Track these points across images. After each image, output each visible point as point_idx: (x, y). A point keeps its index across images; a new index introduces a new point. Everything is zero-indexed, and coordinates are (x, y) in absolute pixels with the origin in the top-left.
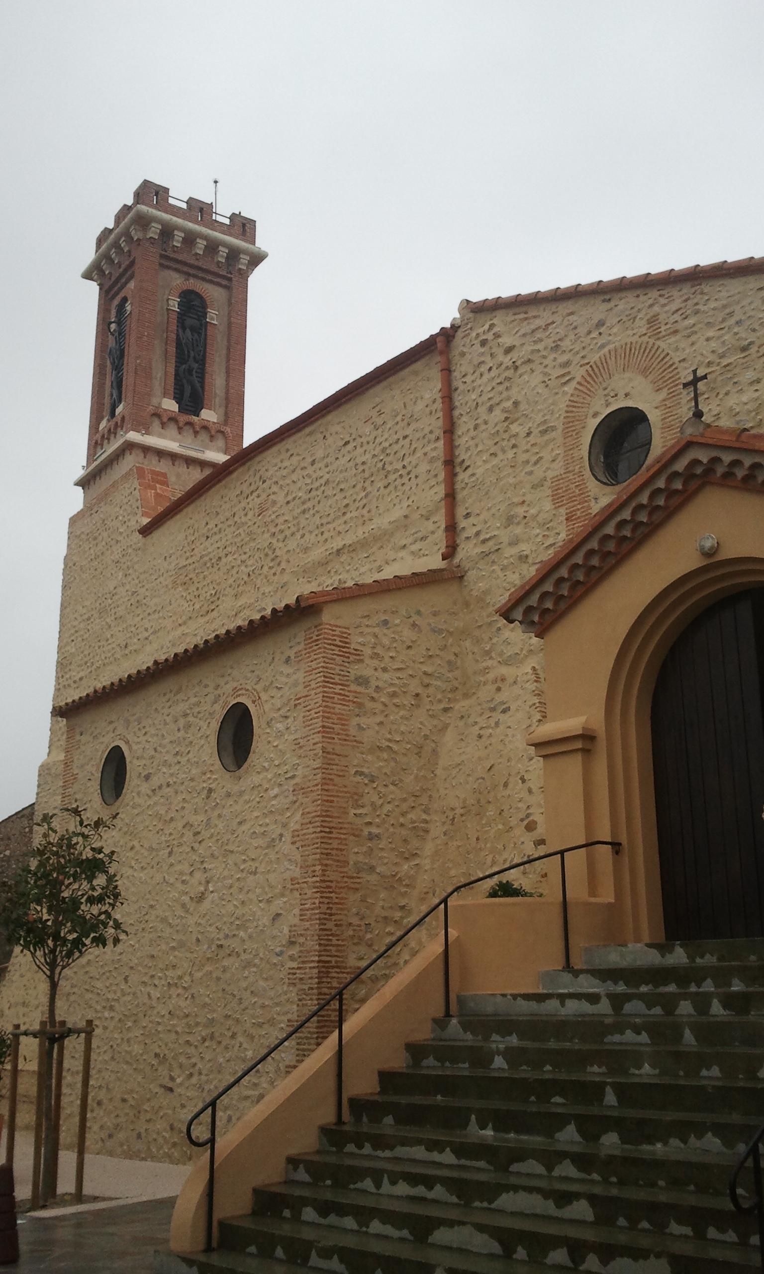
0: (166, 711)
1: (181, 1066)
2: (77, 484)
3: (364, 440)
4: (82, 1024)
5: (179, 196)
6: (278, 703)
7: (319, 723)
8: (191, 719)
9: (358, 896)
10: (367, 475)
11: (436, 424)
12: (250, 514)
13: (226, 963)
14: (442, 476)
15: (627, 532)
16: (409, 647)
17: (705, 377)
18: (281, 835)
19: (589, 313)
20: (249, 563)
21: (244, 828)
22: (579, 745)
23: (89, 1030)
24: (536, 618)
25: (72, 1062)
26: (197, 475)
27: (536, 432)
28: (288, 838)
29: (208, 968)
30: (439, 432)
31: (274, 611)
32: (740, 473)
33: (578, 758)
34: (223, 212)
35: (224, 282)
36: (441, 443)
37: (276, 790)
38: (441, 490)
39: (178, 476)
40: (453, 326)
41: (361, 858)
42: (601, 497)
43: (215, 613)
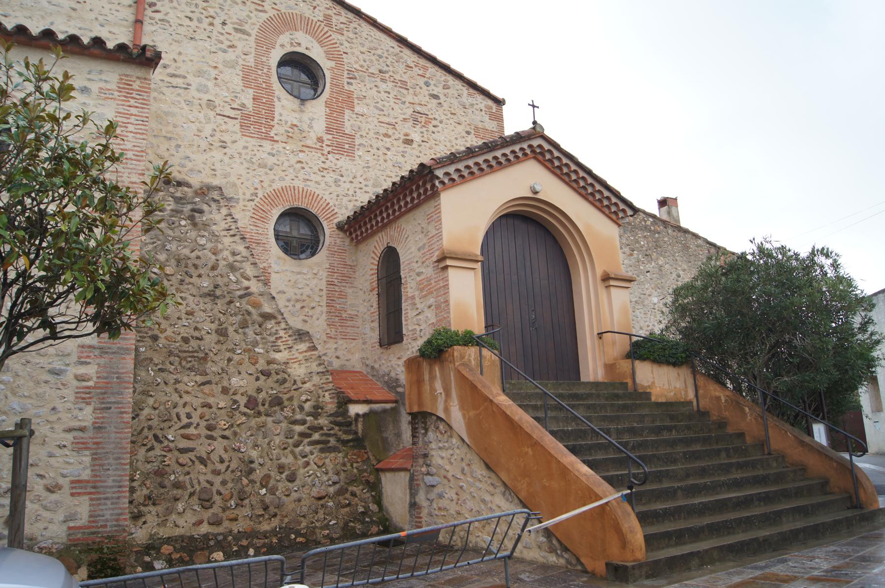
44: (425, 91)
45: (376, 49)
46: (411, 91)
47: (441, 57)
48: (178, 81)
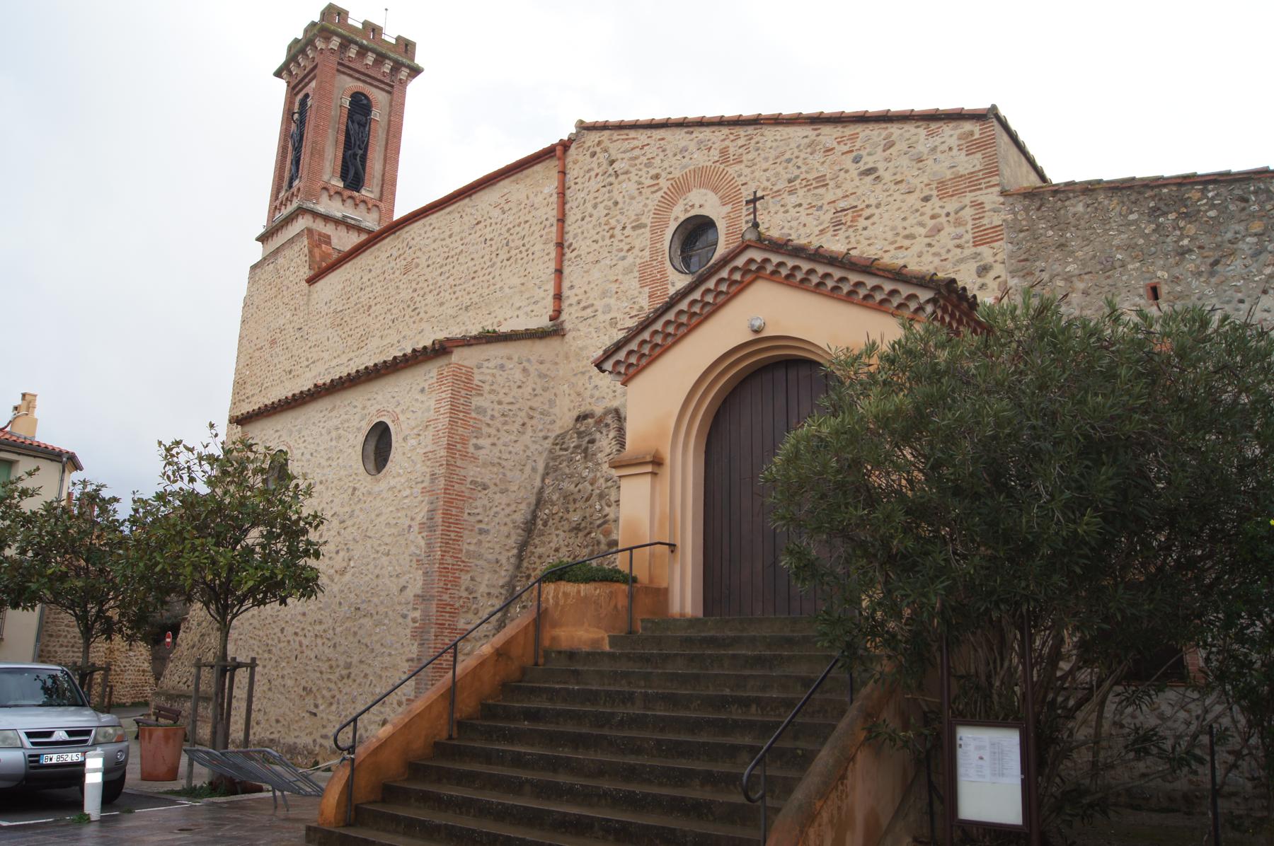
0: (322, 424)
1: (323, 697)
2: (258, 239)
3: (493, 221)
4: (249, 661)
5: (355, 20)
6: (413, 423)
7: (444, 441)
8: (341, 431)
9: (468, 576)
10: (494, 248)
11: (552, 214)
12: (398, 273)
13: (362, 621)
14: (553, 255)
15: (696, 309)
16: (519, 387)
17: (762, 198)
18: (410, 527)
19: (678, 138)
20: (394, 311)
21: (382, 519)
22: (649, 469)
23: (252, 665)
24: (623, 370)
25: (240, 693)
26: (354, 239)
27: (629, 227)
28: (416, 528)
29: (348, 624)
30: (554, 220)
31: (414, 350)
32: (784, 272)
33: (648, 479)
34: (390, 36)
35: (388, 88)
36: (554, 229)
37: (407, 492)
38: (552, 266)
39: (340, 238)
40: (569, 139)
41: (472, 548)
42: (679, 281)
43: (364, 350)
44: (854, 170)
45: (783, 154)
46: (832, 184)
47: (874, 107)
48: (589, 312)
